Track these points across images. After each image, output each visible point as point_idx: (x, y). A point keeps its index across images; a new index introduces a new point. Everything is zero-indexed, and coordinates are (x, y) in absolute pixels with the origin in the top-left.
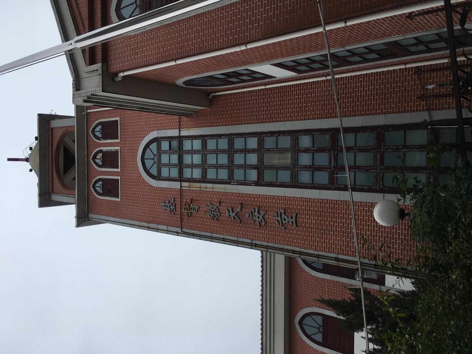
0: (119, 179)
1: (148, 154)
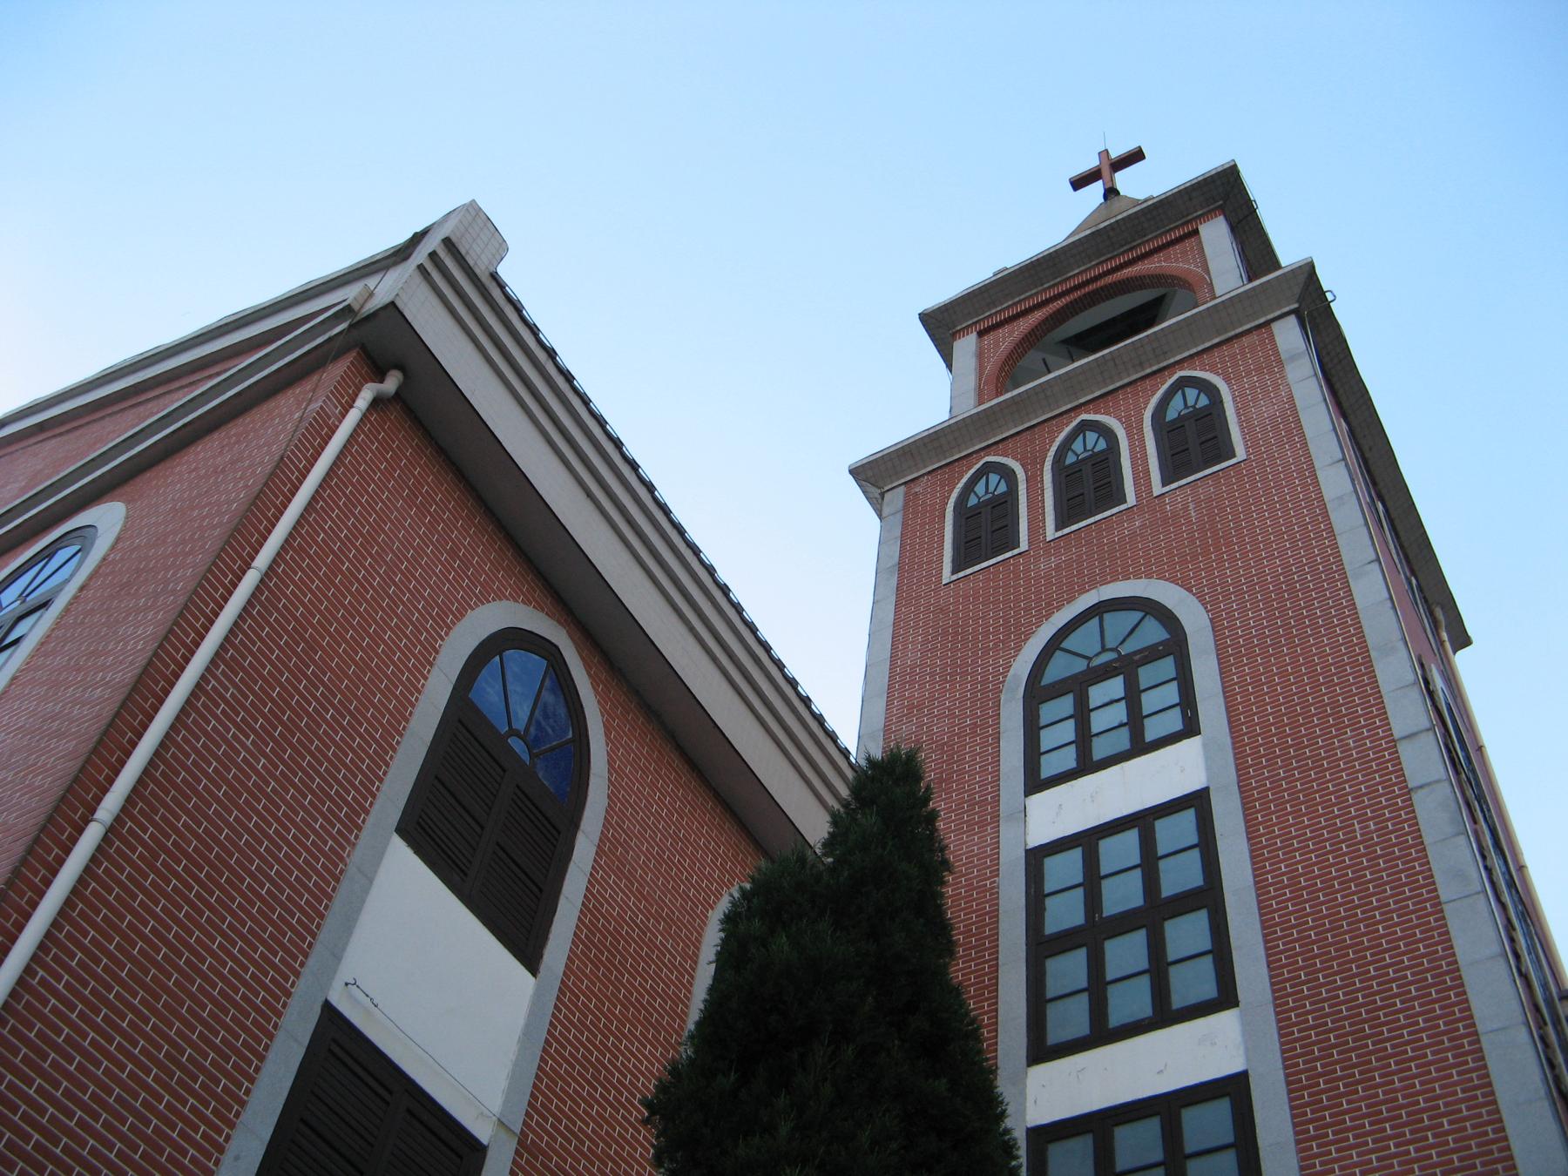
0: (1126, 502)
1: (1118, 623)
